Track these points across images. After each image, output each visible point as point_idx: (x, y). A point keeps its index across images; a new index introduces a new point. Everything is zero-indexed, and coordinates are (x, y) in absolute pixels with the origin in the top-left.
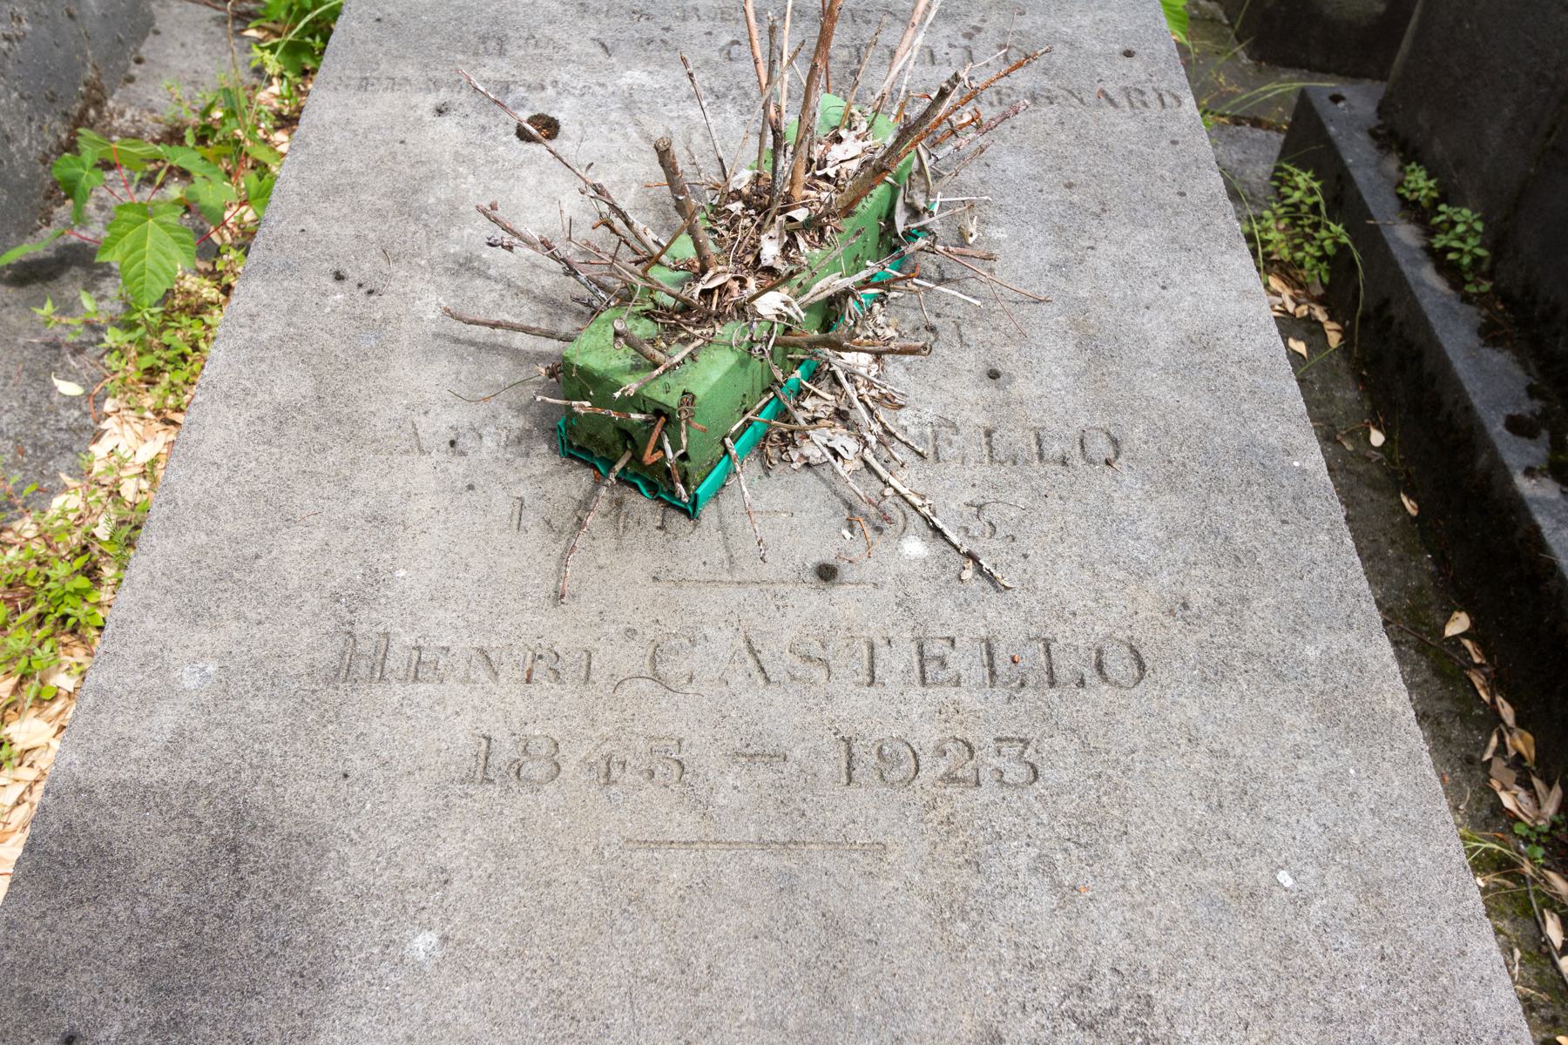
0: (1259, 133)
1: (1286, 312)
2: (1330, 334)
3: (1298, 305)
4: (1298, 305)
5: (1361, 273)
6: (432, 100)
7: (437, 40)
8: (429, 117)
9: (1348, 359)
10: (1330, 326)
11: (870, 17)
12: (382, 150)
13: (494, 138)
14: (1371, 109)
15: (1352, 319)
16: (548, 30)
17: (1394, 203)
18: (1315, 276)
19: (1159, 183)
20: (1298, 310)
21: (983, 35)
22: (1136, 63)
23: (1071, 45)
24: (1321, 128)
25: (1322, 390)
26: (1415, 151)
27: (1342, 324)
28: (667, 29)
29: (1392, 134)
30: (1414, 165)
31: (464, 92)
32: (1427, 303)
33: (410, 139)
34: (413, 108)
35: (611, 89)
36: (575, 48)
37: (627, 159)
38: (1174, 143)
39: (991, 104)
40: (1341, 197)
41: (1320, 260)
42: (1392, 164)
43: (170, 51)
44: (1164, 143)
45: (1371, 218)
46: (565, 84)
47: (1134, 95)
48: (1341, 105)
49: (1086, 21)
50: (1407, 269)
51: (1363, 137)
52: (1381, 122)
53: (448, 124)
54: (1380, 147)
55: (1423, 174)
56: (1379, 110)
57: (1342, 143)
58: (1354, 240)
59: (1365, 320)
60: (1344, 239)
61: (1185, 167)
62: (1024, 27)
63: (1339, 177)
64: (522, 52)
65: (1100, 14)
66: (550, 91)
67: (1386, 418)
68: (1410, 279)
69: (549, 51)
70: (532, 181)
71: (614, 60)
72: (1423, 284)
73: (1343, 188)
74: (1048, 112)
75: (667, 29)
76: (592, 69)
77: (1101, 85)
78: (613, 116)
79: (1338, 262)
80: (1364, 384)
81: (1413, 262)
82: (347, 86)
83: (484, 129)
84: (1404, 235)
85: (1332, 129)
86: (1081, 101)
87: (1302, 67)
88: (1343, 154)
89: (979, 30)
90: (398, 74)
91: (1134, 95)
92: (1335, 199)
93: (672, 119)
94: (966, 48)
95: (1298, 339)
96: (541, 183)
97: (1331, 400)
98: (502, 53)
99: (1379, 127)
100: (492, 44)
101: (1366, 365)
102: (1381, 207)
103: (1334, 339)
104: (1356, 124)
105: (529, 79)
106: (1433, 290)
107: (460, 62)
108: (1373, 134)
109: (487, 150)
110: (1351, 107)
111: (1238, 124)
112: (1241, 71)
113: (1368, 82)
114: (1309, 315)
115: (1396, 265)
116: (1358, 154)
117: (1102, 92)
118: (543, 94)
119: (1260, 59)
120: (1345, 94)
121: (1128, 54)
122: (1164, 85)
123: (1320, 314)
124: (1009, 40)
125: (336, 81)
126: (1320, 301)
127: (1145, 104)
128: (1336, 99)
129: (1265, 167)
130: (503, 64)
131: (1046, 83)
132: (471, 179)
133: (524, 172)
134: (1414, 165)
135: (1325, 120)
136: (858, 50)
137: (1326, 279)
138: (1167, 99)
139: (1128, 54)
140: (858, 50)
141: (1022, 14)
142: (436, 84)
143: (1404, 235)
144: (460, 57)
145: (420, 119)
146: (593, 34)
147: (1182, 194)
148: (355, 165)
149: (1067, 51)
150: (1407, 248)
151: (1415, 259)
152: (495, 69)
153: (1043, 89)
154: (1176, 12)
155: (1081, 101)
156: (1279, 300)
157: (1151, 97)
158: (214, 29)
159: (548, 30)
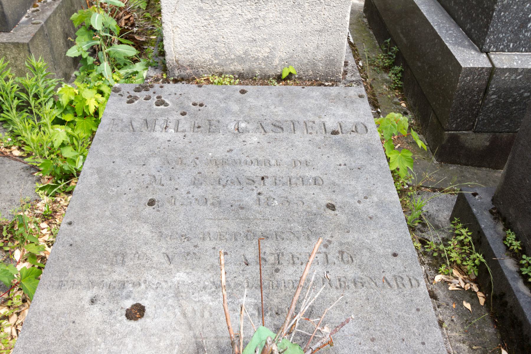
0: (443, 195)
1: (461, 287)
2: (480, 298)
3: (466, 283)
4: (466, 283)
5: (492, 277)
6: (88, 295)
7: (95, 256)
8: (87, 306)
9: (489, 311)
10: (480, 295)
11: (283, 236)
12: (64, 329)
13: (115, 318)
14: (489, 199)
15: (490, 294)
16: (144, 249)
17: (503, 248)
18: (474, 273)
19: (413, 337)
20: (466, 286)
21: (332, 245)
22: (398, 260)
23: (370, 250)
24: (470, 209)
25: (479, 328)
26: (509, 224)
27: (485, 295)
28: (196, 246)
29: (498, 212)
30: (509, 231)
31: (105, 289)
32: (522, 302)
33: (78, 319)
34: (81, 299)
35: (170, 284)
36: (155, 259)
37: (175, 330)
38: (418, 310)
39: (337, 288)
40: (480, 241)
41: (474, 266)
42: (500, 227)
43: (2, 186)
44: (414, 310)
45: (495, 257)
46: (150, 282)
47: (399, 280)
48: (477, 197)
49: (376, 236)
50: (512, 283)
51: (487, 213)
52: (493, 206)
53: (95, 310)
54: (495, 219)
55: (514, 236)
56: (492, 200)
57: (479, 216)
58: (488, 263)
59: (495, 297)
60: (483, 260)
61: (424, 326)
62: (350, 240)
63: (479, 232)
64: (132, 263)
65: (382, 231)
66: (143, 286)
67: (508, 345)
68: (514, 288)
69: (144, 261)
70: (130, 346)
71: (172, 266)
72: (520, 291)
73: (481, 237)
74: (362, 292)
75: (196, 246)
76: (162, 273)
77: (384, 274)
78: (170, 302)
79: (481, 267)
80: (497, 325)
81: (514, 279)
82: (53, 286)
83: (111, 312)
84: (508, 264)
85: (474, 210)
86: (376, 283)
87: (458, 164)
88: (480, 222)
89: (330, 242)
90: (76, 279)
91: (399, 280)
92: (478, 240)
93: (196, 302)
94: (325, 253)
95: (467, 302)
96: (134, 347)
97: (483, 334)
98: (123, 263)
99: (493, 208)
100: (119, 258)
101: (497, 317)
102: (497, 248)
103: (482, 301)
104: (484, 207)
105: (134, 279)
106: (524, 294)
107: (105, 270)
108: (491, 212)
109: (112, 326)
110: (480, 198)
111: (435, 192)
112: (434, 167)
113: (484, 169)
114: (471, 288)
115: (507, 280)
116: (486, 222)
117: (384, 278)
118: (139, 289)
119: (441, 162)
120: (478, 192)
121: (395, 255)
122: (411, 274)
123: (475, 289)
124: (344, 248)
125: (48, 283)
126: (475, 281)
127: (403, 285)
128: (475, 195)
129: (447, 213)
130: (123, 270)
131: (360, 274)
132: (103, 346)
133: (127, 340)
134: (509, 231)
135: (471, 205)
136: (278, 256)
137: (477, 274)
138: (414, 282)
139: (395, 255)
140: (278, 256)
141: (348, 232)
142: (92, 284)
143: (508, 264)
144: (105, 267)
145: (83, 307)
146: (164, 250)
147: (423, 343)
148: (50, 339)
149: (368, 254)
150: (511, 271)
151: (514, 277)
152: (120, 274)
153: (359, 278)
154: (409, 159)
155: (376, 283)
156: (457, 281)
157: (406, 281)
158: (22, 173)
159: (144, 249)
